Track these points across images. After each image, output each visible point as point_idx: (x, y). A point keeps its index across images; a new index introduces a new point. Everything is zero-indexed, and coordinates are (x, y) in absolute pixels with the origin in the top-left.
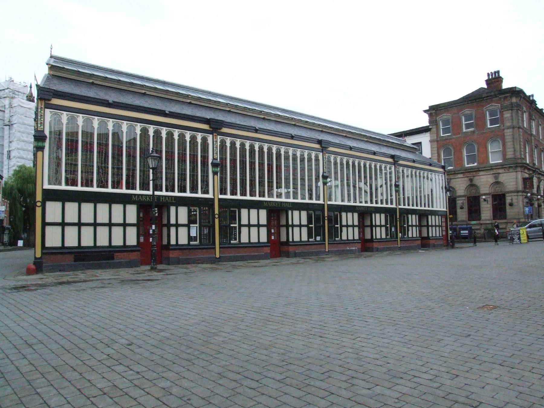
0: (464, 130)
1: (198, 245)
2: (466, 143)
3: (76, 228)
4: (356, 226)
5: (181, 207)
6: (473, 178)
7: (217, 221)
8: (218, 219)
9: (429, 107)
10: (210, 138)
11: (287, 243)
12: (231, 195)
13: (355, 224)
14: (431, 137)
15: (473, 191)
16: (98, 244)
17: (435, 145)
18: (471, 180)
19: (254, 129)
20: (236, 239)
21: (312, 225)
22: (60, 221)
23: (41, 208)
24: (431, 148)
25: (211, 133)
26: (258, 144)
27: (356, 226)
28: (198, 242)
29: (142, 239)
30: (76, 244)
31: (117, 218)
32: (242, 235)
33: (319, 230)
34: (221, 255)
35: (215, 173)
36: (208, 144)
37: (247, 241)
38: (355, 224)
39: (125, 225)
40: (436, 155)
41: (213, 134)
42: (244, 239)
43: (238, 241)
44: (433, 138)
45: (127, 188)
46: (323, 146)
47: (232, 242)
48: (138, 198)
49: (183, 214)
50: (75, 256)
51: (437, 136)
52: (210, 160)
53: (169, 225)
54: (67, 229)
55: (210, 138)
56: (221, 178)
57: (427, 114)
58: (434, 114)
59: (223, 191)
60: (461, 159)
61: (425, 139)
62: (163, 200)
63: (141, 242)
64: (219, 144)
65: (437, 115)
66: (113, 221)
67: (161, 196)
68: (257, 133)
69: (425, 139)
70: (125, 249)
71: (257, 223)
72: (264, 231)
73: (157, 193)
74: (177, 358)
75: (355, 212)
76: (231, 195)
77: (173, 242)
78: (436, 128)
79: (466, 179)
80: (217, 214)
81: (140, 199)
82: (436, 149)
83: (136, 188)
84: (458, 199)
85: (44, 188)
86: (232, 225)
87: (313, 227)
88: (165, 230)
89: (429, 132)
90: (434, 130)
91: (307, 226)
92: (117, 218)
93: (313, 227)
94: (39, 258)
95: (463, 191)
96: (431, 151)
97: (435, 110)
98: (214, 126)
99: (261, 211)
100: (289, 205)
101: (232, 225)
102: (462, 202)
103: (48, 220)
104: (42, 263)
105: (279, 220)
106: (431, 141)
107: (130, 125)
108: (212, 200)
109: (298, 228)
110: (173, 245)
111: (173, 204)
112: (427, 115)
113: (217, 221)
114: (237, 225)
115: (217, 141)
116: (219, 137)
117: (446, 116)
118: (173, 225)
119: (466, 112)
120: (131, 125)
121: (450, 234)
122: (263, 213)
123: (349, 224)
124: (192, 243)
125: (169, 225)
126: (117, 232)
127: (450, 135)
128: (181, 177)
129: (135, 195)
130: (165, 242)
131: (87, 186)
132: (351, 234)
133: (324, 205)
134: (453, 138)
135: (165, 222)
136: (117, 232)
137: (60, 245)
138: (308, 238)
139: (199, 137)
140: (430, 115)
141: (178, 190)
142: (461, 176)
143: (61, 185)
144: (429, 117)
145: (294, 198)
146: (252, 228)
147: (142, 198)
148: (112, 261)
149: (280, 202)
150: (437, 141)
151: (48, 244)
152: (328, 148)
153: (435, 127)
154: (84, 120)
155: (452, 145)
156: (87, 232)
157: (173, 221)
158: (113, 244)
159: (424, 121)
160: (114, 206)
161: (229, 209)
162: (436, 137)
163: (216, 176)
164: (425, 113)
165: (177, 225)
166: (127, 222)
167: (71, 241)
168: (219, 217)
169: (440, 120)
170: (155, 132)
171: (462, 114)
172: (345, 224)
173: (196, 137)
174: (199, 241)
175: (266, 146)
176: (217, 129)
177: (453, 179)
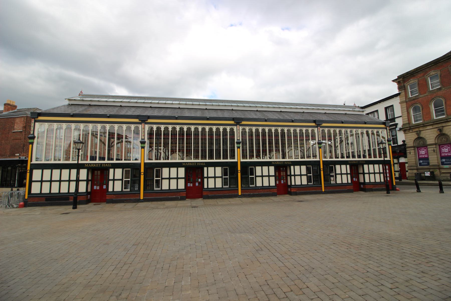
0: (431, 89)
1: (312, 185)
2: (433, 99)
3: (261, 178)
4: (349, 174)
5: (54, 170)
6: (443, 129)
7: (322, 172)
8: (322, 171)
9: (398, 77)
10: (316, 130)
11: (364, 183)
12: (358, 158)
13: (381, 172)
14: (400, 100)
15: (444, 139)
16: (171, 188)
17: (405, 105)
18: (440, 130)
19: (265, 119)
20: (126, 189)
21: (254, 175)
22: (261, 175)
23: (29, 173)
24: (401, 108)
25: (236, 125)
26: (355, 130)
27: (349, 174)
28: (228, 186)
29: (278, 183)
30: (39, 192)
31: (265, 173)
32: (337, 179)
33: (317, 177)
34: (325, 190)
35: (238, 147)
36: (234, 132)
37: (374, 181)
38: (381, 172)
39: (269, 176)
40: (406, 113)
41: (317, 127)
42: (259, 184)
43: (255, 185)
44: (402, 100)
45: (374, 158)
46: (317, 123)
47: (251, 186)
48: (185, 164)
49: (119, 173)
50: (46, 198)
51: (406, 98)
52: (236, 141)
53: (291, 176)
54: (376, 175)
55: (316, 130)
56: (243, 150)
57: (396, 82)
58: (401, 82)
59: (244, 156)
60: (429, 113)
61: (396, 102)
62: (103, 166)
63: (89, 192)
64: (321, 132)
65: (404, 82)
66: (302, 174)
67: (103, 163)
68: (266, 122)
69: (396, 102)
70: (177, 191)
71: (168, 177)
72: (272, 179)
73: (386, 159)
74: (268, 244)
75: (348, 164)
76: (358, 158)
77: (293, 184)
78: (405, 92)
79: (436, 129)
80: (28, 173)
81: (187, 165)
82: (406, 108)
83: (355, 157)
84: (428, 147)
85: (145, 162)
86: (331, 174)
87: (228, 178)
88: (289, 178)
89: (399, 96)
90: (403, 93)
91: (306, 175)
92: (265, 173)
93: (228, 178)
94: (27, 199)
95: (434, 140)
96: (402, 110)
97: (403, 78)
98: (236, 121)
99: (270, 167)
100: (290, 163)
101: (331, 174)
102: (433, 149)
103: (257, 175)
104: (27, 202)
105: (357, 170)
106: (401, 103)
107: (111, 126)
108: (319, 162)
109: (373, 175)
110: (293, 185)
111: (112, 168)
112: (396, 83)
113: (322, 172)
114: (334, 174)
115: (320, 131)
116: (321, 128)
117: (413, 81)
118: (293, 175)
119: (431, 73)
120: (112, 126)
121: (396, 178)
122: (272, 169)
123: (302, 174)
124: (309, 184)
125: (291, 176)
126: (266, 179)
127: (418, 95)
128: (189, 152)
129: (184, 163)
130: (289, 184)
131: (157, 159)
132: (346, 179)
133: (319, 161)
134: (421, 97)
135: (289, 174)
136: (266, 179)
137: (168, 188)
138: (308, 182)
139: (228, 128)
140: (399, 83)
141: (357, 157)
142: (431, 127)
143: (235, 159)
144: (398, 85)
145: (369, 158)
146: (71, 183)
147: (188, 164)
148: (68, 201)
149: (283, 161)
150: (406, 102)
151: (33, 192)
152: (321, 125)
153: (403, 91)
154: (149, 127)
155: (420, 103)
156: (173, 182)
157: (292, 173)
158: (61, 192)
159: (394, 89)
160: (370, 165)
161: (329, 166)
162: (405, 99)
163: (320, 149)
164: (394, 82)
165: (295, 175)
166: (263, 175)
167: (46, 190)
168: (241, 172)
169: (408, 85)
170: (255, 130)
171: (427, 76)
172: (112, 178)
173: (168, 128)
174: (229, 186)
175: (310, 129)
176: (240, 123)
177: (422, 131)
